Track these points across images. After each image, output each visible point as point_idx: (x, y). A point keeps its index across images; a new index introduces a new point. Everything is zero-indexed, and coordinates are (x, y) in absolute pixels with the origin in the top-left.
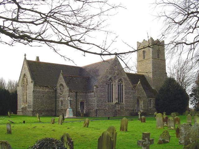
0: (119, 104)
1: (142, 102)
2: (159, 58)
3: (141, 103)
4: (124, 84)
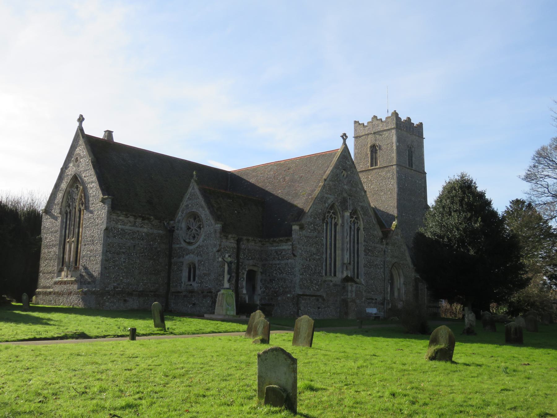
1: (402, 280)
2: (412, 166)
4: (361, 225)
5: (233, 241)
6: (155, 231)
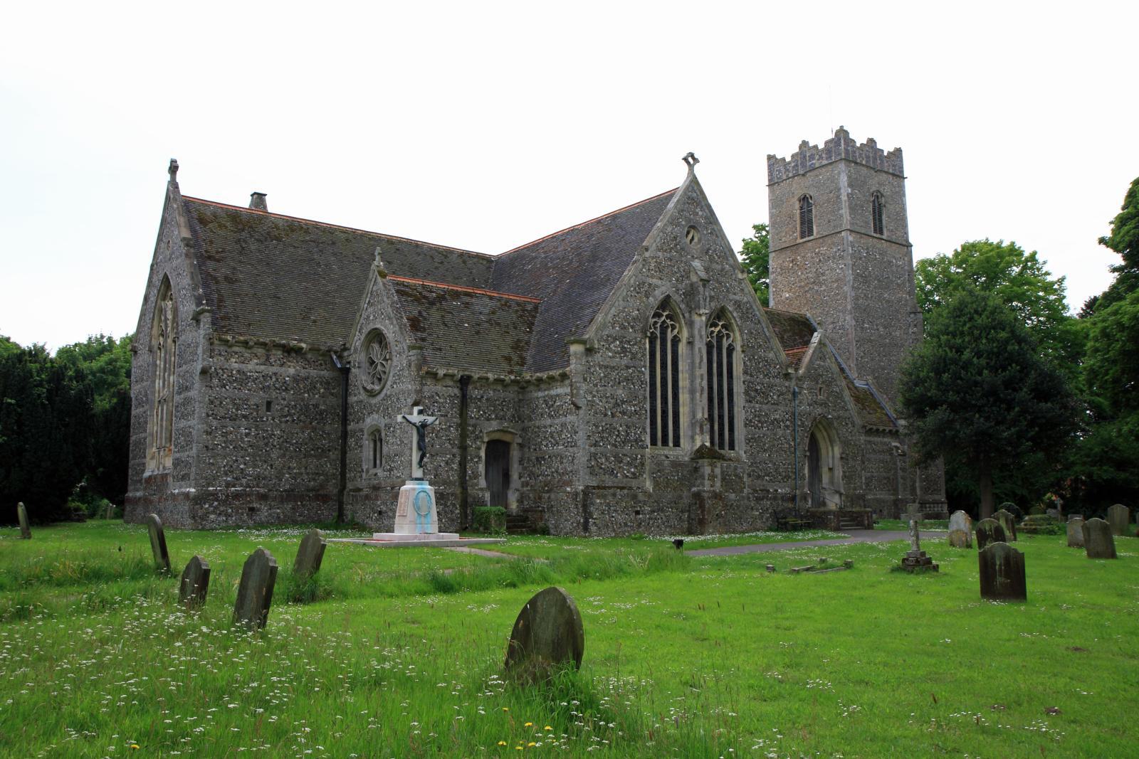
0: (722, 458)
1: (837, 451)
2: (881, 233)
3: (832, 454)
4: (738, 339)
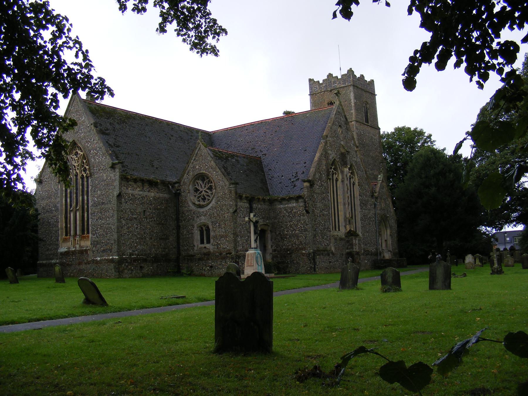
2: (368, 123)
5: (246, 201)
6: (161, 195)
